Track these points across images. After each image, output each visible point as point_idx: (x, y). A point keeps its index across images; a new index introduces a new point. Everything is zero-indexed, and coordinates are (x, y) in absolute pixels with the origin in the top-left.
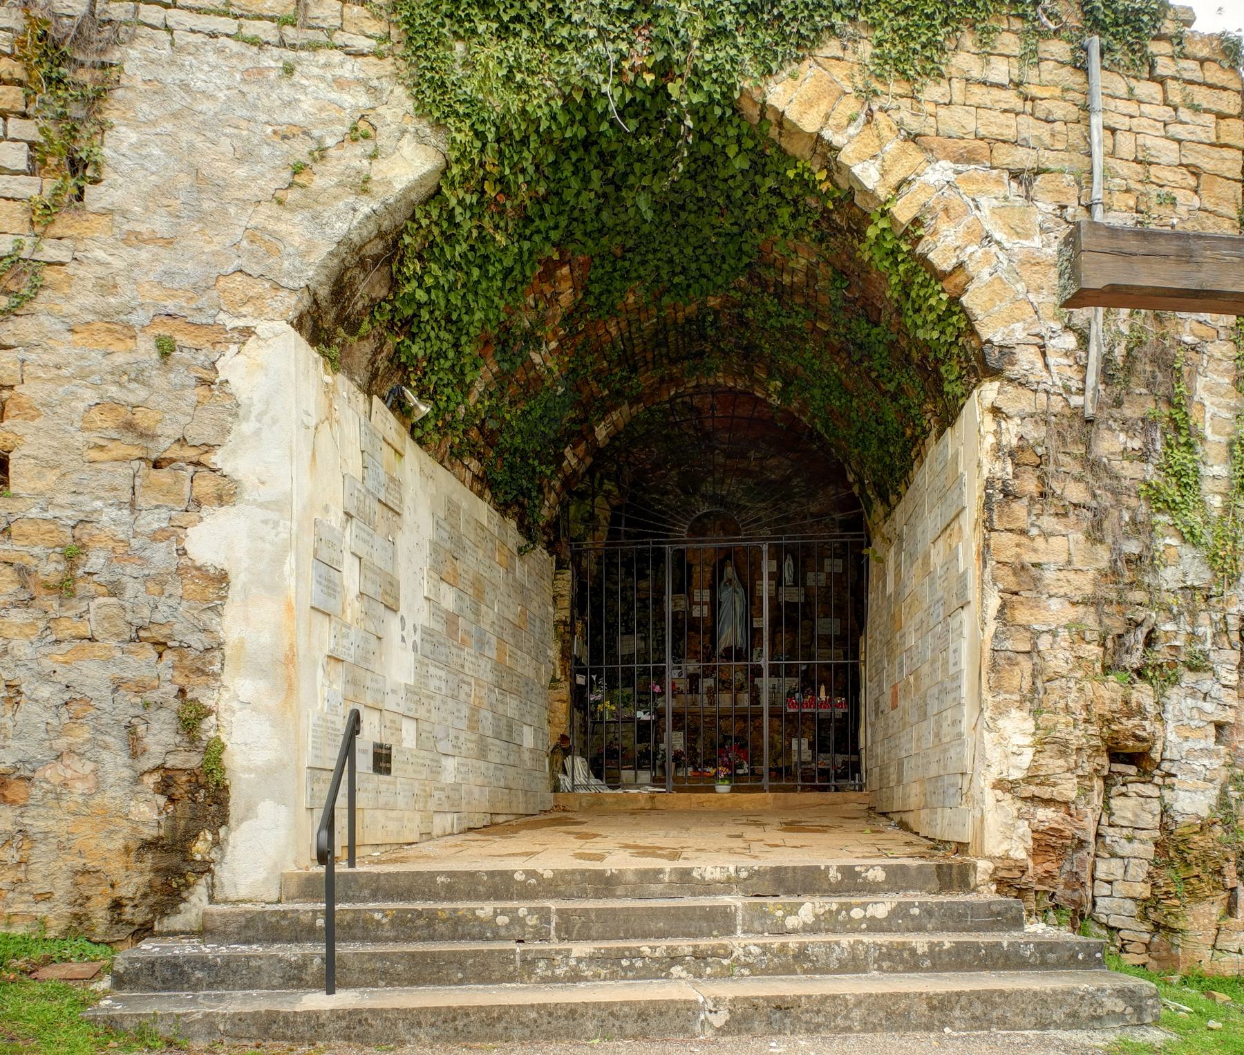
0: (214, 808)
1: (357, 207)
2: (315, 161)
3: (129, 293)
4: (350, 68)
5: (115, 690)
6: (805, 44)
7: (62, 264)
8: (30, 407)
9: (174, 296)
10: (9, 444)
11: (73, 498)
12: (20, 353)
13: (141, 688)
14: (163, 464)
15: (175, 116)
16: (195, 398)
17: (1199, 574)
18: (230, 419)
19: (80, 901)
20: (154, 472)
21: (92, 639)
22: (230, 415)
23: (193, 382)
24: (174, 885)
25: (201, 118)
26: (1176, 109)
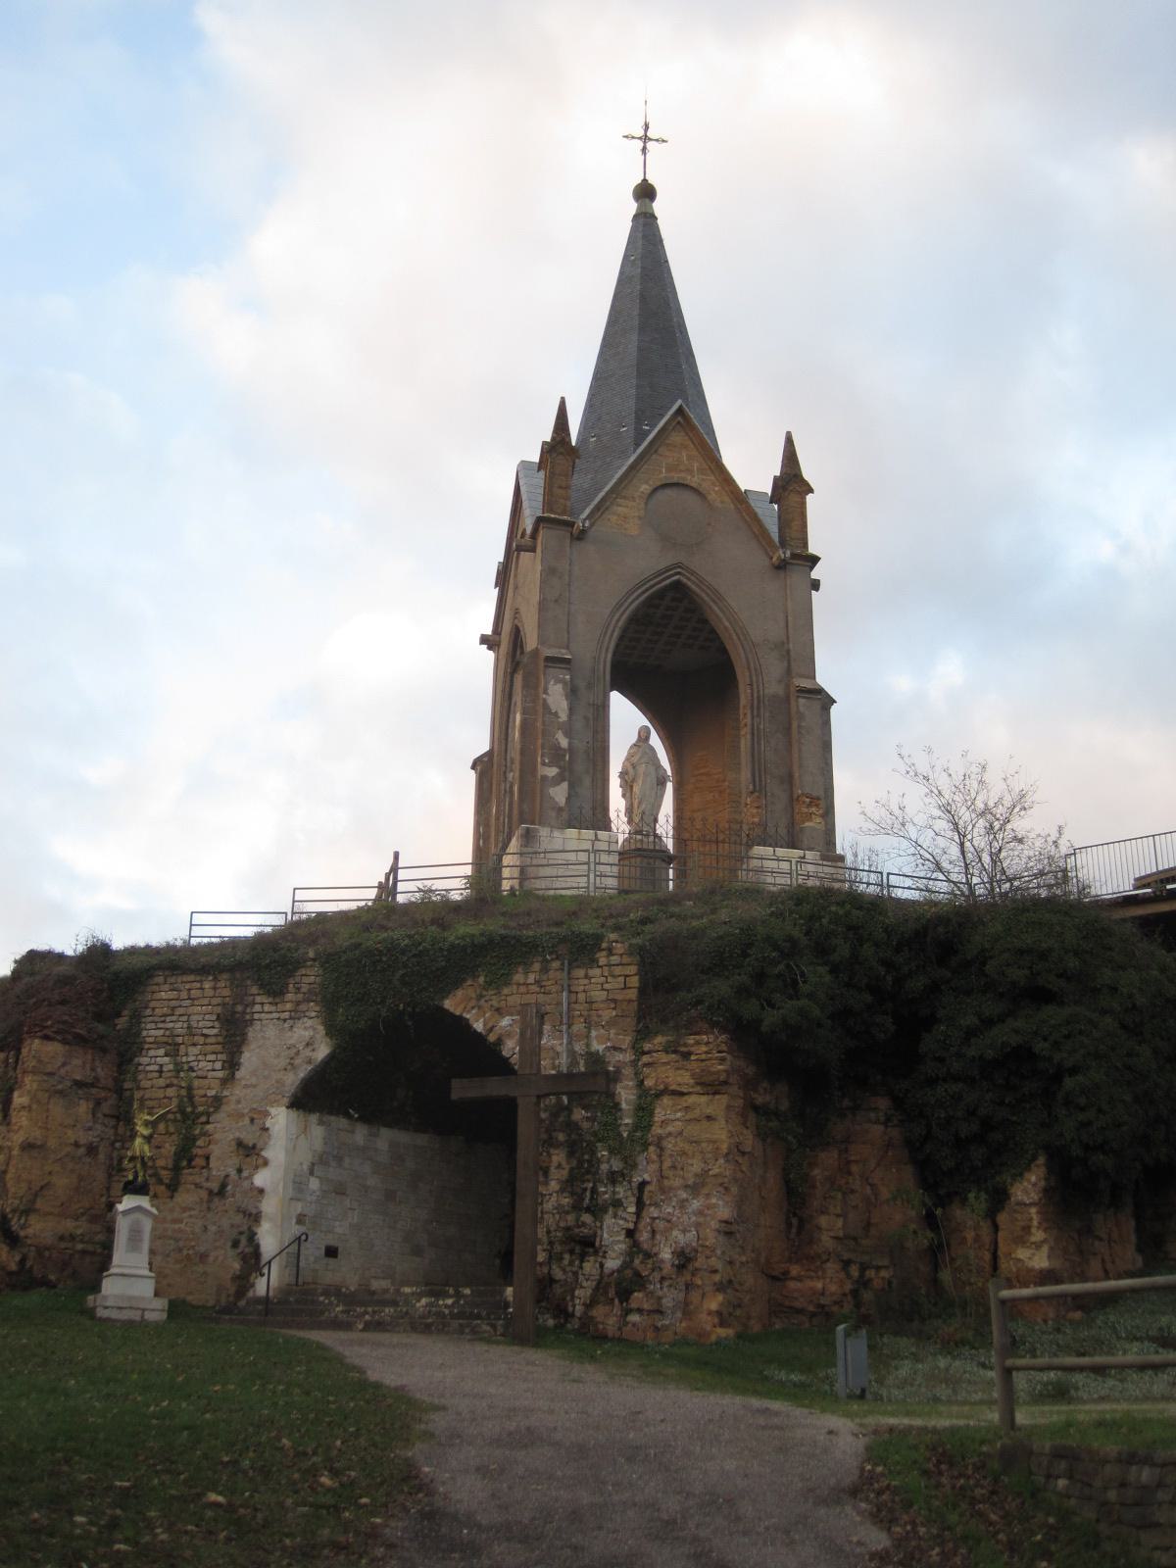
4: (309, 1023)
6: (457, 984)
12: (215, 1125)
13: (239, 1226)
15: (259, 1047)
17: (617, 1165)
26: (606, 977)
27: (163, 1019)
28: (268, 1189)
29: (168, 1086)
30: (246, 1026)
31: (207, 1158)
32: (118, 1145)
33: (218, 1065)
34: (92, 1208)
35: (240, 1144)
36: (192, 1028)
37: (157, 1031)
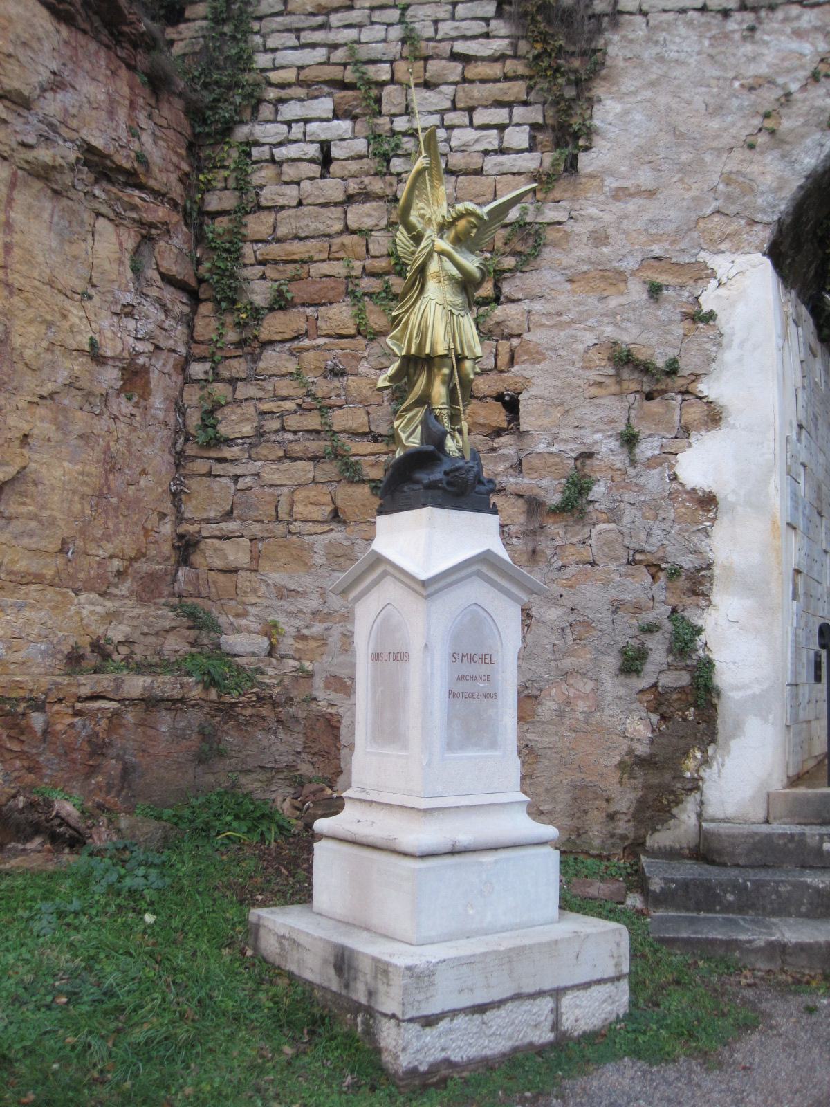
0: (703, 726)
1: (823, 141)
2: (782, 105)
3: (619, 242)
5: (615, 612)
7: (560, 223)
8: (537, 352)
9: (660, 241)
10: (519, 387)
11: (575, 433)
12: (526, 305)
13: (638, 608)
14: (655, 394)
15: (652, 84)
16: (681, 332)
18: (714, 349)
19: (578, 814)
20: (647, 403)
21: (593, 564)
22: (715, 345)
23: (679, 317)
24: (665, 802)
25: (676, 82)
27: (320, 19)
28: (726, 490)
29: (350, 199)
30: (599, 31)
31: (511, 405)
32: (197, 369)
33: (518, 137)
34: (140, 555)
35: (624, 360)
36: (420, 38)
37: (299, 53)
